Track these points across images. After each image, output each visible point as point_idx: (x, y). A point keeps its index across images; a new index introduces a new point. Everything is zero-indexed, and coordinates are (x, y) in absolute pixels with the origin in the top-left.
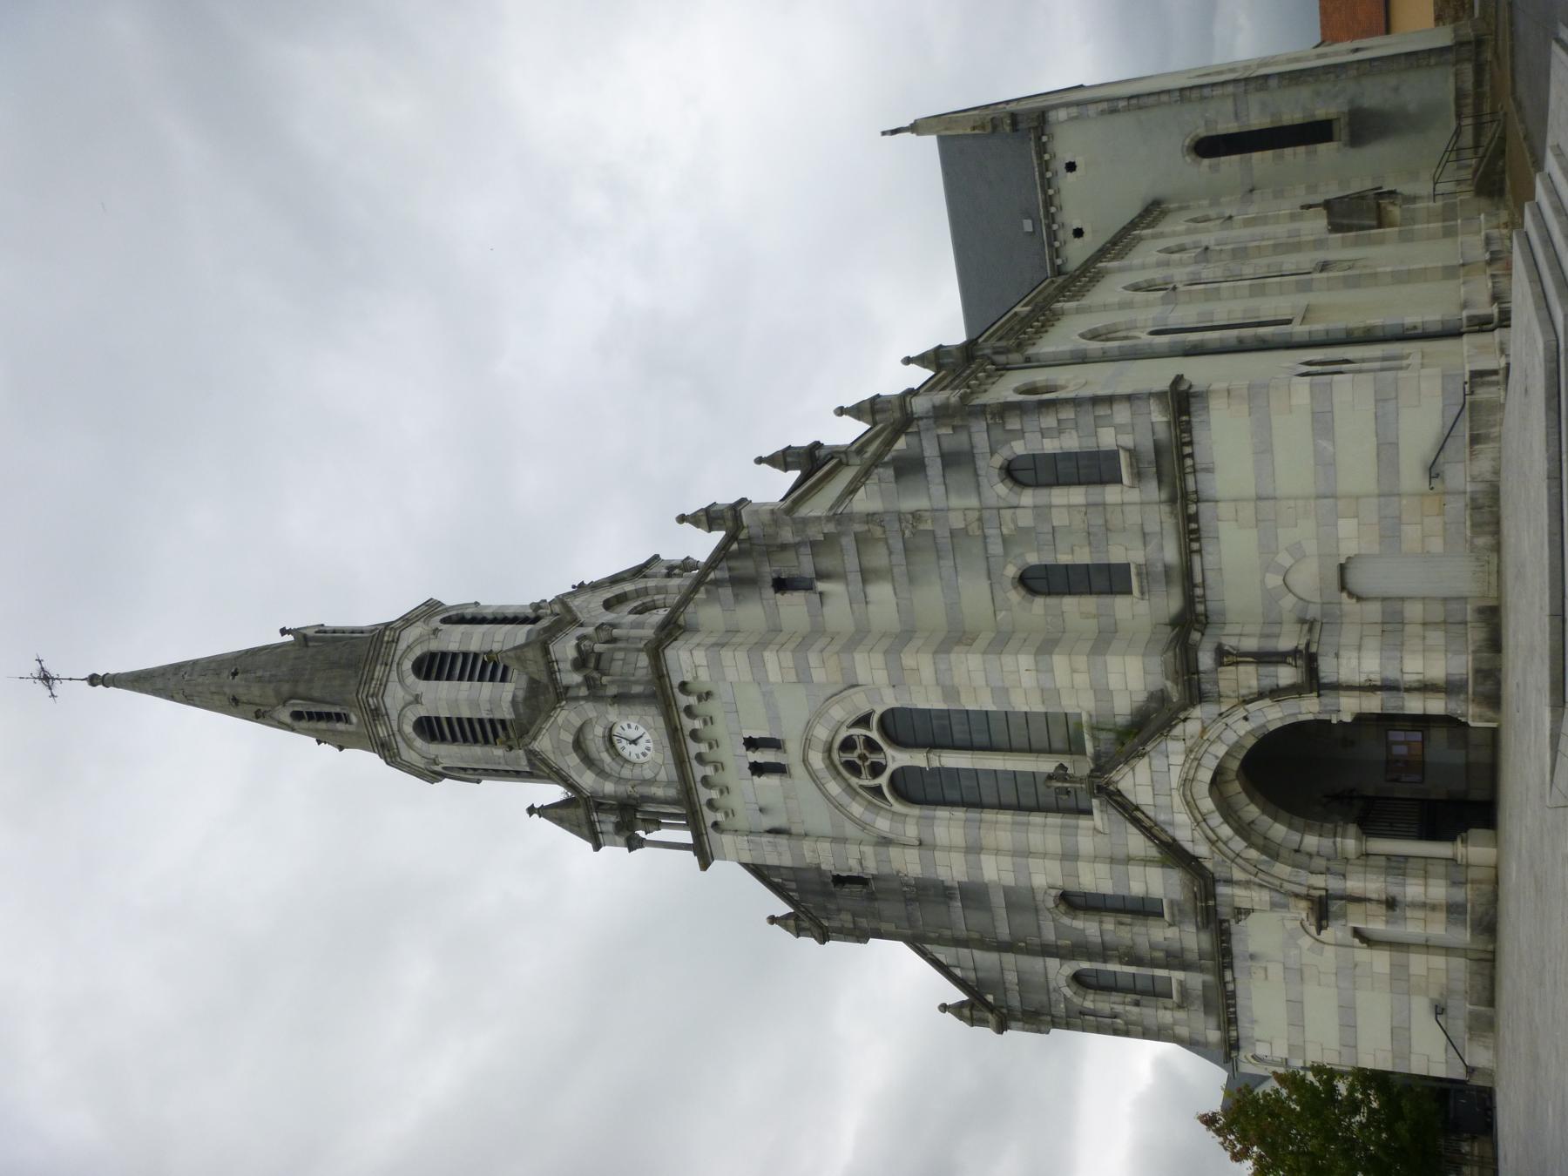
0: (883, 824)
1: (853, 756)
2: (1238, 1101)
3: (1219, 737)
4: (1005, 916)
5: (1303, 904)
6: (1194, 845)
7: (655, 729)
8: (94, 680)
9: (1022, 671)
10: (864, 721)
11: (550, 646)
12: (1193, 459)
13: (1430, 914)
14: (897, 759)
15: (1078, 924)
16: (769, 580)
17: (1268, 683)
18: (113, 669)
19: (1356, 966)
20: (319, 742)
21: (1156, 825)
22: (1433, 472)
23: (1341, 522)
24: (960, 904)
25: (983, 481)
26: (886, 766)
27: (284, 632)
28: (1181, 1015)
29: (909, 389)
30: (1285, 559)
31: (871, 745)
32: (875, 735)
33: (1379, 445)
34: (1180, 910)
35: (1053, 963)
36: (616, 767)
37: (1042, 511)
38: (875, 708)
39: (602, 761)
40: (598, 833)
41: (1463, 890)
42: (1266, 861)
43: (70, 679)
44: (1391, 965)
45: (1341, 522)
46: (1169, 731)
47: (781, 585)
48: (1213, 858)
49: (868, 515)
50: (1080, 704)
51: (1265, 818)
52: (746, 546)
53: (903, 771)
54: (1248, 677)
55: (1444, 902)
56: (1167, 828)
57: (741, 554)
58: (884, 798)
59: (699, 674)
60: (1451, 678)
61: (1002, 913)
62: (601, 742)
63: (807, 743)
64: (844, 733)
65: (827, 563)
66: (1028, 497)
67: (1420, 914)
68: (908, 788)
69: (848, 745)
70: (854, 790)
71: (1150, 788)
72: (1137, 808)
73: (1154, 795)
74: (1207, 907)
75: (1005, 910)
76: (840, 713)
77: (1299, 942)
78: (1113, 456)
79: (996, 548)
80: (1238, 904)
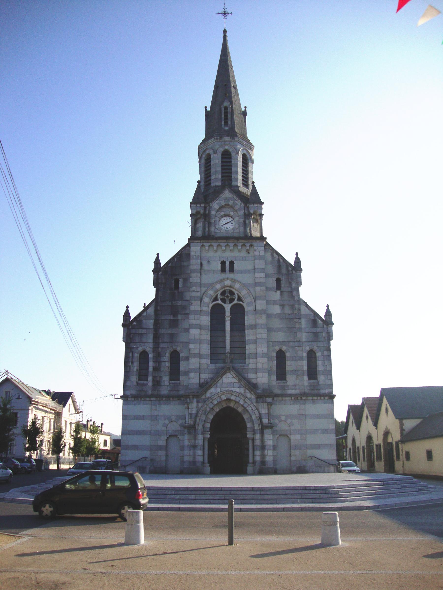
0: (206, 300)
1: (227, 294)
2: (159, 404)
3: (246, 402)
4: (168, 332)
5: (192, 423)
6: (210, 393)
7: (233, 232)
8: (225, 32)
9: (262, 349)
10: (240, 299)
12: (323, 399)
14: (228, 307)
15: (167, 355)
16: (280, 277)
17: (263, 416)
18: (228, 38)
21: (217, 383)
23: (300, 435)
24: (171, 318)
25: (309, 343)
26: (225, 304)
27: (245, 107)
28: (135, 384)
29: (154, 285)
30: (289, 421)
31: (232, 300)
32: (235, 302)
33: (319, 445)
35: (151, 345)
36: (219, 216)
37: (301, 358)
38: (245, 303)
39: (221, 212)
40: (196, 205)
43: (225, 23)
45: (300, 435)
46: (247, 389)
47: (278, 281)
48: (206, 398)
49: (300, 309)
50: (251, 363)
51: (215, 413)
52: (291, 272)
53: (224, 309)
54: (264, 411)
56: (215, 386)
57: (288, 270)
58: (213, 301)
59: (257, 252)
60: (266, 462)
61: (169, 331)
62: (228, 213)
63: (234, 281)
64: (236, 292)
65: (286, 295)
66: (305, 355)
67: (192, 454)
69: (232, 293)
70: (216, 292)
71: (228, 382)
72: (222, 378)
73: (226, 383)
74: (190, 396)
75: (170, 332)
76: (243, 293)
78: (316, 378)
79: (291, 344)
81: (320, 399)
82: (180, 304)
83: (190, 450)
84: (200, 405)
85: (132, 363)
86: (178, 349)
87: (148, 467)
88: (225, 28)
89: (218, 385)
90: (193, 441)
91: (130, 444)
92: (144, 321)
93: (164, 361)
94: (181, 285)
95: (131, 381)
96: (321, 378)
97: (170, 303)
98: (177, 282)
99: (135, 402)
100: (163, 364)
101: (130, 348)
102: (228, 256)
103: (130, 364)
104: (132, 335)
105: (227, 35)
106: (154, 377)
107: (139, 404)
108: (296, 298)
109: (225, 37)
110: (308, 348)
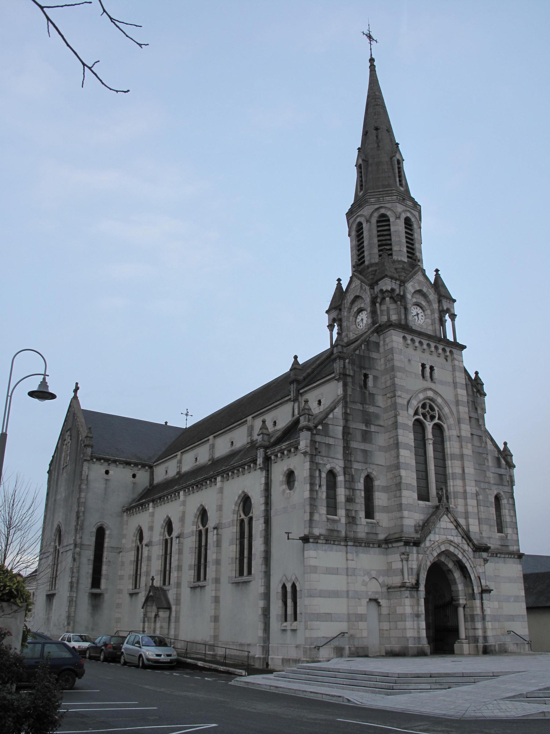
8: (372, 60)
11: (386, 279)
13: (416, 631)
15: (362, 480)
19: (359, 599)
20: (359, 149)
22: (509, 632)
31: (432, 418)
34: (373, 526)
35: (341, 463)
41: (426, 643)
42: (427, 568)
44: (361, 614)
55: (421, 636)
67: (416, 627)
68: (419, 426)
69: (432, 409)
74: (410, 542)
77: (366, 576)
80: (410, 554)
81: (511, 558)
82: (372, 411)
83: (414, 621)
84: (421, 556)
85: (320, 486)
86: (374, 474)
87: (347, 647)
88: (371, 55)
89: (437, 530)
90: (416, 608)
91: (322, 611)
92: (331, 426)
93: (359, 488)
94: (370, 383)
95: (319, 514)
96: (509, 531)
97: (359, 407)
98: (366, 376)
99: (327, 546)
100: (358, 492)
101: (316, 463)
102: (430, 360)
103: (318, 487)
104: (317, 444)
105: (375, 64)
106: (347, 510)
107: (331, 550)
108: (483, 429)
109: (372, 68)
110: (495, 492)
